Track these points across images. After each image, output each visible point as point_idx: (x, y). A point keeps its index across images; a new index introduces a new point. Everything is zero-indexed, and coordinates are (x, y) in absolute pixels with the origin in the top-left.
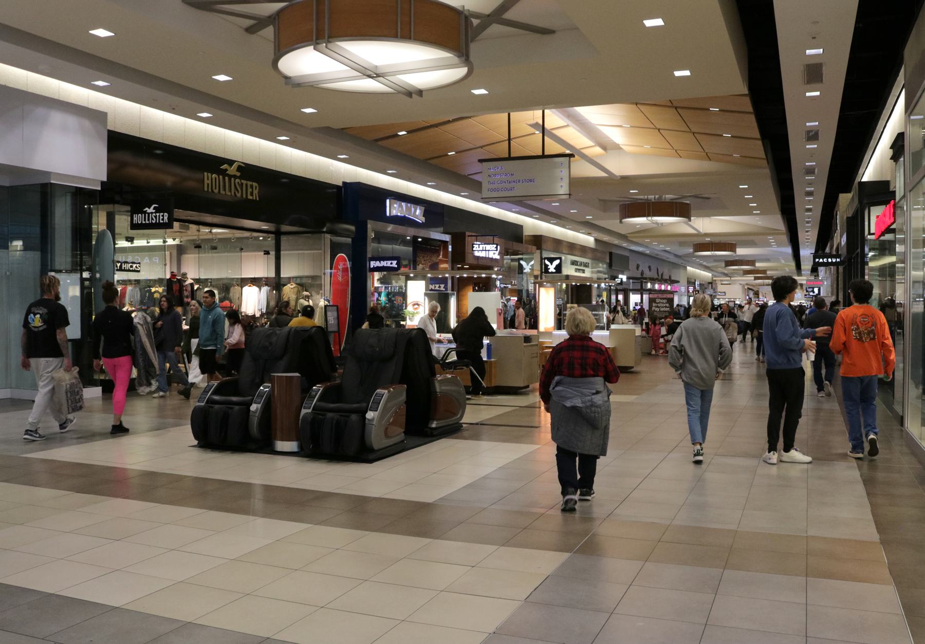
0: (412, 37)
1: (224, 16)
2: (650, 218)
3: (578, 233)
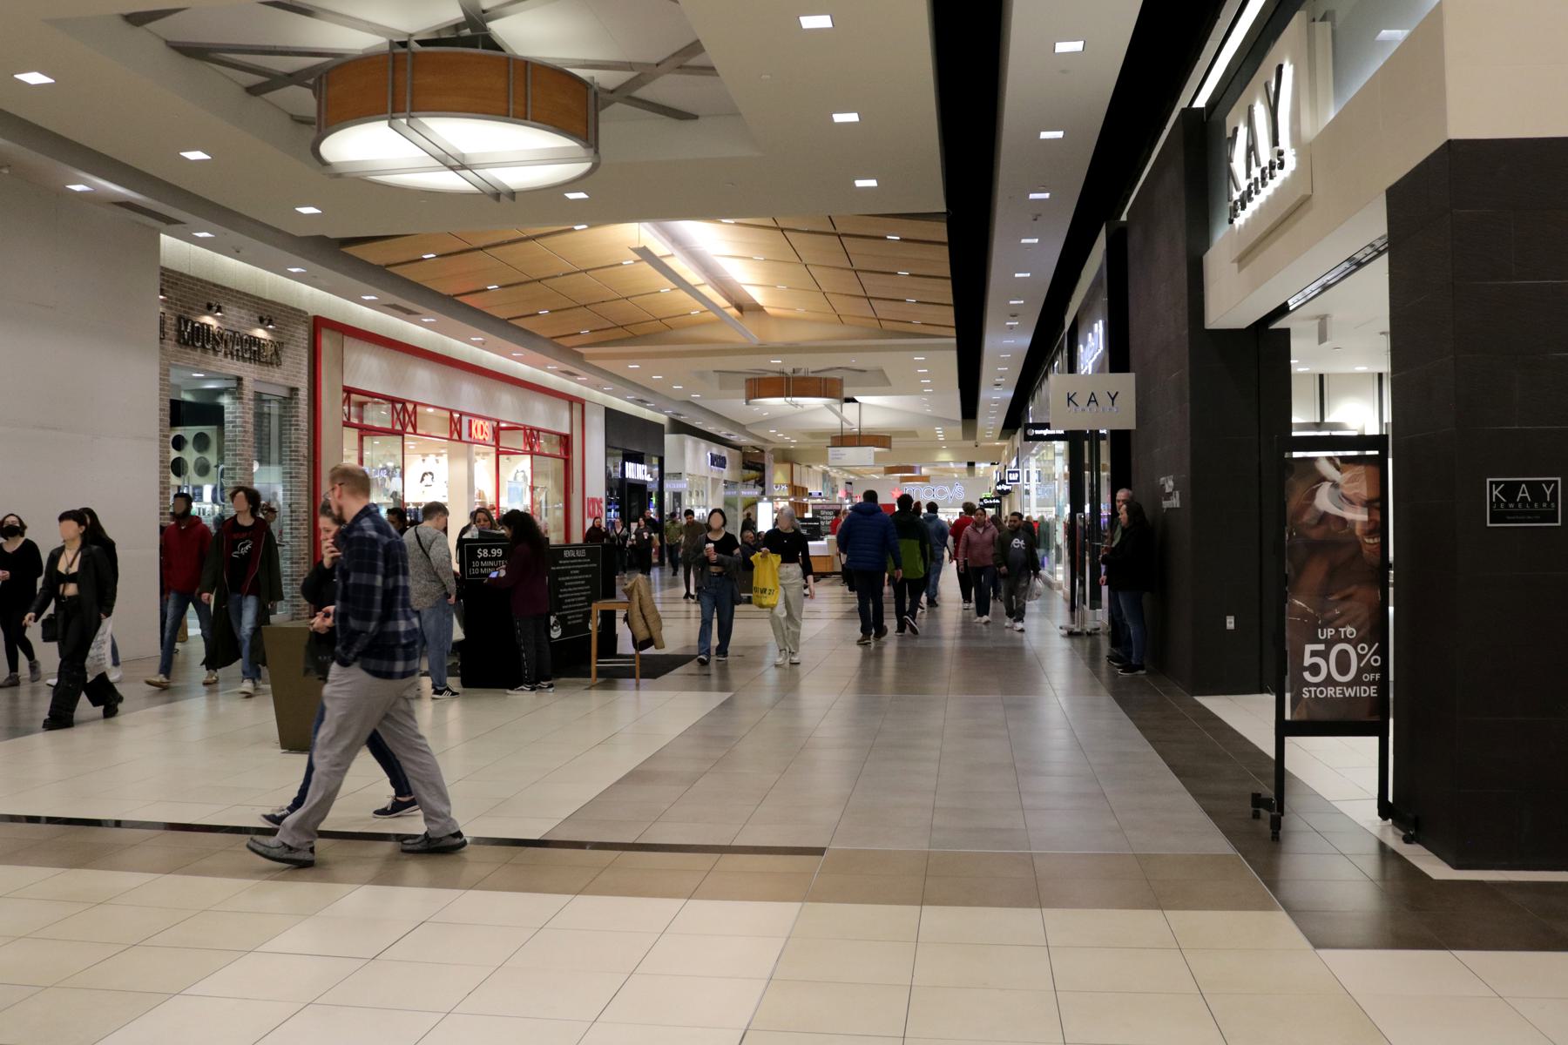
0: (529, 116)
2: (789, 399)
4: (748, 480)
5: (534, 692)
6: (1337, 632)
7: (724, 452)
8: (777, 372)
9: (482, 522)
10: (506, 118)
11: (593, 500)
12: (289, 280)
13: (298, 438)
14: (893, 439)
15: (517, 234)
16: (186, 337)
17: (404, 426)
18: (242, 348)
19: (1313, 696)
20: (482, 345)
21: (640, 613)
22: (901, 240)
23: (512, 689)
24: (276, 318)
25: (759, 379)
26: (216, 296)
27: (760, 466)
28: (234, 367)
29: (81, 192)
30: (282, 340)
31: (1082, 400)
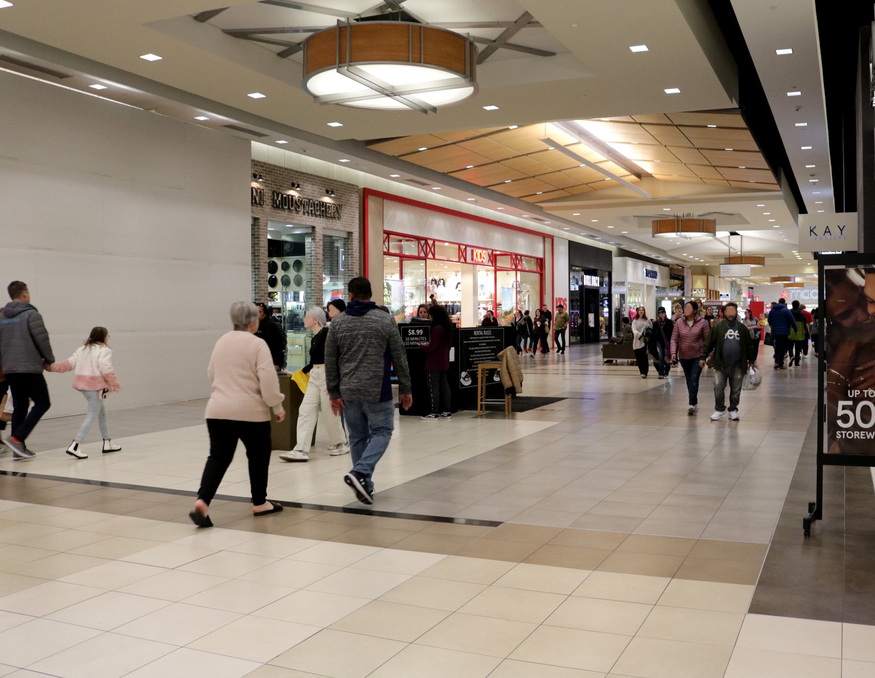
1: (256, 42)
2: (679, 233)
3: (386, 180)
4: (673, 286)
5: (437, 419)
6: (862, 392)
7: (656, 268)
8: (672, 216)
9: (423, 313)
10: (420, 64)
11: (560, 299)
12: (349, 169)
13: (353, 263)
14: (766, 259)
15: (473, 133)
16: (278, 203)
17: (426, 255)
18: (314, 209)
19: (844, 437)
20: (475, 203)
21: (506, 371)
22: (717, 127)
23: (424, 416)
24: (337, 190)
25: (660, 221)
26: (297, 178)
27: (681, 277)
28: (310, 220)
29: (203, 121)
30: (341, 203)
31: (820, 231)
